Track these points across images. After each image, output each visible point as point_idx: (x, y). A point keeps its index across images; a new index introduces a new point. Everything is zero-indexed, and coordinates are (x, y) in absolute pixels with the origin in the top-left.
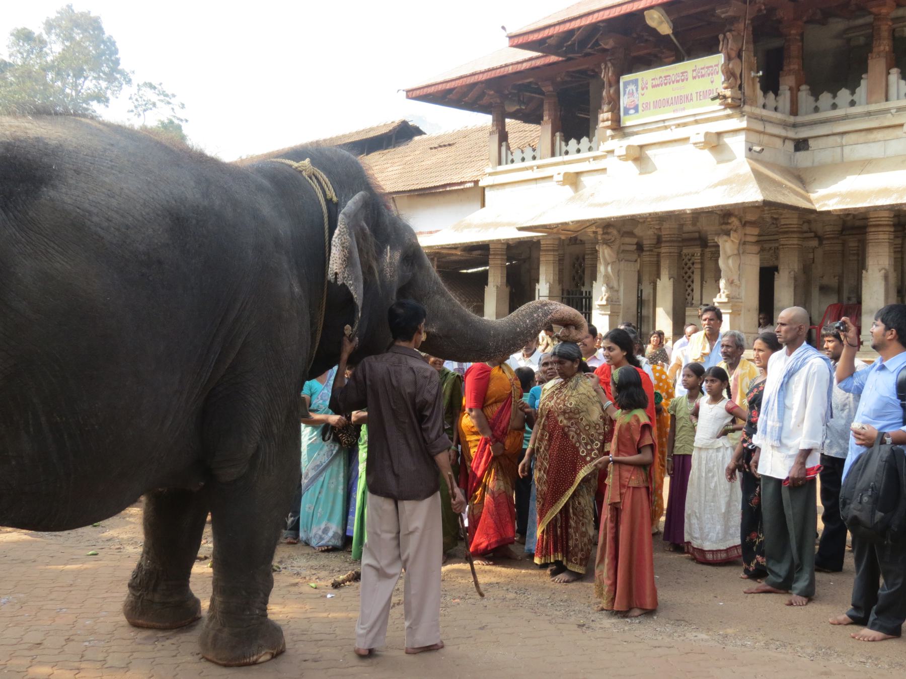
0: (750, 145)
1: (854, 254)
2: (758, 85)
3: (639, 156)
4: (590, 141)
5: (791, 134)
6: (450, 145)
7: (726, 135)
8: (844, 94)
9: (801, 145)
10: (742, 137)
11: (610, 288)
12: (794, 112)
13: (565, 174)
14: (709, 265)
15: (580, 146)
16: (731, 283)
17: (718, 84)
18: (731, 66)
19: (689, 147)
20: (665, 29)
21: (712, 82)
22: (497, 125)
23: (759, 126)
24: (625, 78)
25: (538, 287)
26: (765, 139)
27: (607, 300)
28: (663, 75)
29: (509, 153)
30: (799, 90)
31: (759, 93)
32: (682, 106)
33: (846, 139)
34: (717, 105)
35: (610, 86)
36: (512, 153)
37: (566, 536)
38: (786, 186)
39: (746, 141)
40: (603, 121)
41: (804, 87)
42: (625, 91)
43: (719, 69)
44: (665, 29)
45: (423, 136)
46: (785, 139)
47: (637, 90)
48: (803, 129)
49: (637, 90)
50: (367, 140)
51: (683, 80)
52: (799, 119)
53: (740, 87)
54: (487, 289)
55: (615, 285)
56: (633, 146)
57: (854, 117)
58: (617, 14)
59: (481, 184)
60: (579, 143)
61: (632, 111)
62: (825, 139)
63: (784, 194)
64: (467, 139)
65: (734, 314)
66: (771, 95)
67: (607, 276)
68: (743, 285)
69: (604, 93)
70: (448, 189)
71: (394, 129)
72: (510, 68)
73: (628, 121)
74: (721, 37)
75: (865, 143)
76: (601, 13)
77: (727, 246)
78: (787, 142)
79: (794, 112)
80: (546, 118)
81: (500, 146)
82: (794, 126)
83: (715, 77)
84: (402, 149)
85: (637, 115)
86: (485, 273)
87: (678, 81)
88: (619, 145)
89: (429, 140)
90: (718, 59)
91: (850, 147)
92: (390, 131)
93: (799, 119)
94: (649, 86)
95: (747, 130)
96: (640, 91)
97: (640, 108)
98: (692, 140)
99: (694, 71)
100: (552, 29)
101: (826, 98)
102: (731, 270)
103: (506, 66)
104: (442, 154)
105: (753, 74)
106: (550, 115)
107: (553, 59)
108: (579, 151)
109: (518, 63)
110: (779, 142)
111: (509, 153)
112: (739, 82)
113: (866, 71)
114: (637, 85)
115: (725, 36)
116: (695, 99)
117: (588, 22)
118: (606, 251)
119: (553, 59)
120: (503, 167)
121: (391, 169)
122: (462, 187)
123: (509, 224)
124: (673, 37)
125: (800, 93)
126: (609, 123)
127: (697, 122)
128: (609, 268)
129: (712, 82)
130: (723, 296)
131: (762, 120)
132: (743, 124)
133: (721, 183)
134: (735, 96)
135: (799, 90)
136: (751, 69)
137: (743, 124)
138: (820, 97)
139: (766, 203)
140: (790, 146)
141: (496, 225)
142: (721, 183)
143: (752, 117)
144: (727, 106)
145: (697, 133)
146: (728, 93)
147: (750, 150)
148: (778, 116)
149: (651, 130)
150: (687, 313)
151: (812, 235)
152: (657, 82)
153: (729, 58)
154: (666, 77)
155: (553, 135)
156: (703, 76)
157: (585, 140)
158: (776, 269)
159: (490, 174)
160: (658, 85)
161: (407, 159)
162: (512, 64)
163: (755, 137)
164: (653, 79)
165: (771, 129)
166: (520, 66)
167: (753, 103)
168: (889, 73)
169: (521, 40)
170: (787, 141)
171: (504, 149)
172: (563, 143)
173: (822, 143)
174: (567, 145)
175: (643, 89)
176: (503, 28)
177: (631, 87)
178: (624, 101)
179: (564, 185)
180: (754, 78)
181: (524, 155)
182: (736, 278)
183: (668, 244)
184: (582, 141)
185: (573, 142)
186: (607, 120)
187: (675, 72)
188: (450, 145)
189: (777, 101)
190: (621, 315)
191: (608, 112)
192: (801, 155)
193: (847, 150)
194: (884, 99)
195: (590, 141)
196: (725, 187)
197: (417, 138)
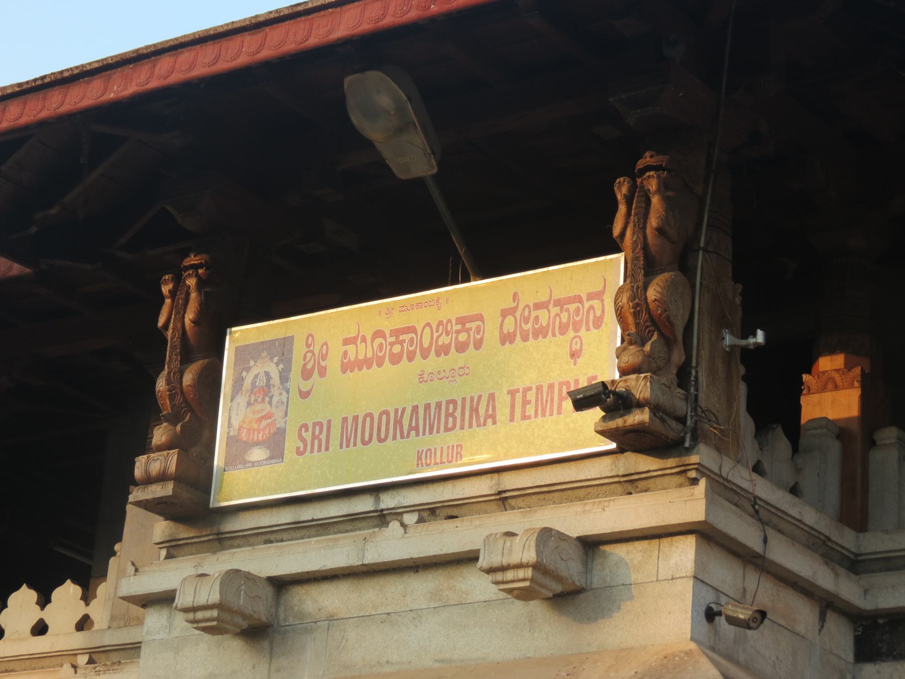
0: (709, 597)
4: (87, 598)
5: (848, 590)
10: (683, 554)
15: (49, 615)
17: (602, 355)
18: (652, 293)
19: (475, 585)
20: (412, 157)
21: (574, 355)
24: (239, 336)
26: (766, 593)
28: (387, 326)
30: (873, 443)
31: (747, 424)
32: (450, 439)
35: (187, 358)
37: (176, 295)
40: (149, 481)
41: (889, 435)
42: (238, 383)
44: (412, 157)
46: (827, 604)
47: (284, 378)
48: (891, 578)
49: (284, 378)
51: (462, 348)
52: (875, 543)
53: (684, 376)
58: (243, 60)
60: (44, 601)
61: (258, 454)
69: (161, 385)
73: (240, 481)
74: (622, 189)
76: (186, 56)
79: (855, 511)
83: (589, 337)
87: (443, 350)
88: (196, 577)
90: (608, 272)
94: (333, 363)
95: (705, 534)
96: (296, 379)
97: (291, 443)
98: (483, 562)
99: (505, 313)
105: (729, 339)
108: (40, 629)
110: (804, 614)
112: (678, 356)
116: (503, 412)
124: (436, 194)
125: (876, 456)
126: (163, 490)
127: (503, 500)
129: (574, 355)
131: (757, 510)
132: (689, 504)
134: (663, 400)
135: (873, 443)
136: (721, 322)
137: (689, 504)
143: (721, 489)
144: (629, 441)
145: (512, 537)
146: (640, 387)
147: (711, 615)
149: (323, 527)
152: (362, 351)
153: (645, 267)
154: (396, 333)
156: (541, 332)
157: (67, 593)
160: (366, 363)
163: (727, 574)
164: (346, 342)
175: (306, 374)
178: (231, 416)
180: (728, 356)
186: (162, 478)
187: (432, 316)
189: (798, 470)
191: (168, 446)
195: (87, 598)
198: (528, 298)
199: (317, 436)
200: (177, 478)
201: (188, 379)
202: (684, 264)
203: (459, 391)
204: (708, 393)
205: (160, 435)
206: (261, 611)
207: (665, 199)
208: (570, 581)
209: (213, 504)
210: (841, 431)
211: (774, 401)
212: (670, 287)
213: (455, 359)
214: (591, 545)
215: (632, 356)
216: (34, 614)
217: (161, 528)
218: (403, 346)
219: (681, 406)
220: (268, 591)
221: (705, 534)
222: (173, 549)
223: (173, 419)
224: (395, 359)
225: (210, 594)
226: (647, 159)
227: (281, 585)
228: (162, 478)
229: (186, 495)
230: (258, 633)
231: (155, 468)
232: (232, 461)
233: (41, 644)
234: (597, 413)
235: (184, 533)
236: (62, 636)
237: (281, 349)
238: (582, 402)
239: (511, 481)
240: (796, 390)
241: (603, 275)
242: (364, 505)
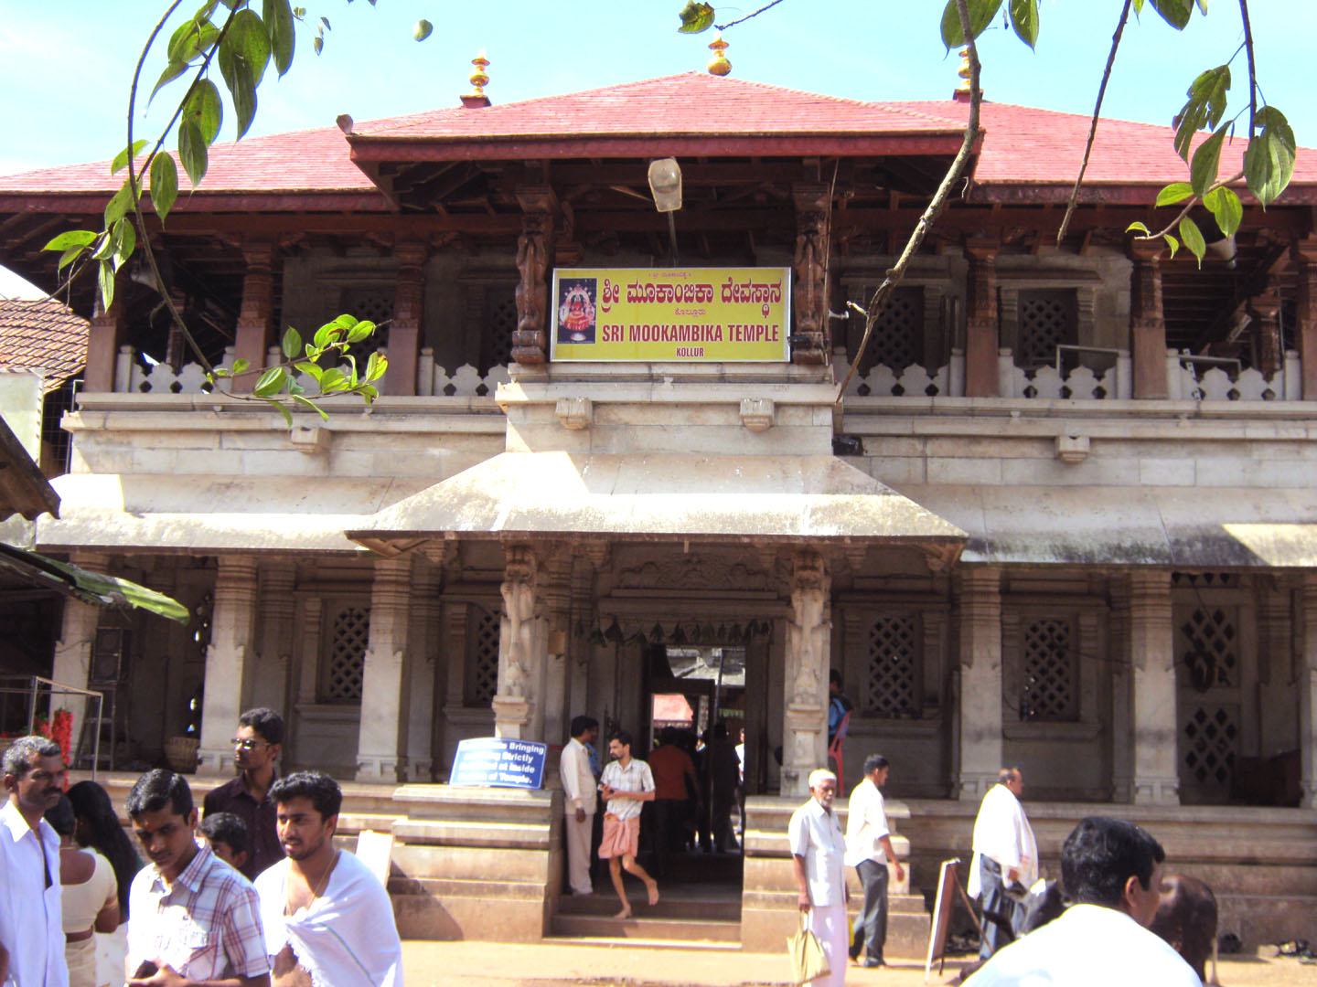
1: (312, 623)
7: (791, 411)
8: (915, 376)
20: (669, 202)
33: (931, 448)
44: (669, 202)
49: (592, 299)
52: (1207, 406)
55: (528, 665)
57: (931, 412)
67: (519, 646)
75: (967, 457)
77: (516, 603)
85: (589, 346)
87: (689, 299)
91: (941, 460)
94: (623, 296)
97: (599, 333)
138: (872, 371)
151: (774, 596)
155: (117, 352)
156: (745, 299)
168: (419, 354)
172: (441, 371)
173: (888, 447)
175: (606, 300)
183: (392, 588)
193: (934, 465)
194: (109, 385)
239: (729, 371)
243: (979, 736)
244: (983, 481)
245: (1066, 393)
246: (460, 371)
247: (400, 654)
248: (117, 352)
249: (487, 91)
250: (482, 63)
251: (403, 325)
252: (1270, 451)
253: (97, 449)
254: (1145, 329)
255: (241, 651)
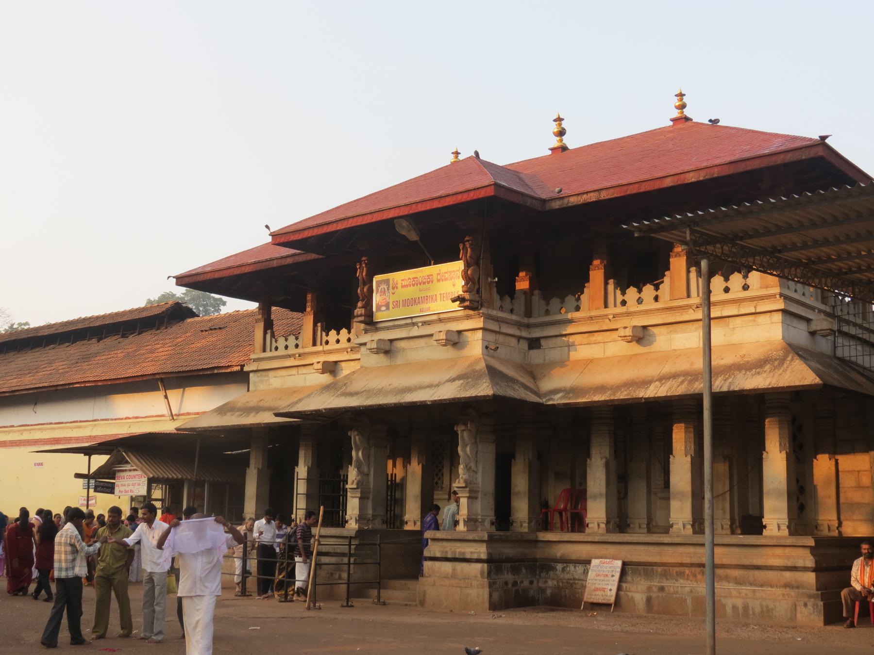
0: (486, 343)
2: (495, 290)
3: (387, 349)
4: (349, 332)
5: (525, 334)
6: (220, 328)
9: (534, 344)
10: (479, 334)
11: (360, 472)
12: (528, 313)
13: (325, 362)
14: (658, 481)
15: (340, 337)
16: (468, 468)
18: (469, 272)
22: (263, 314)
23: (494, 326)
24: (376, 279)
25: (297, 469)
26: (501, 338)
27: (357, 484)
28: (411, 277)
29: (274, 340)
31: (496, 297)
34: (456, 306)
35: (364, 285)
36: (276, 341)
38: (518, 381)
39: (483, 340)
40: (358, 316)
41: (536, 292)
42: (377, 289)
43: (460, 274)
44: (413, 236)
45: (196, 319)
46: (519, 338)
50: (139, 319)
51: (428, 283)
52: (532, 321)
53: (478, 291)
54: (248, 471)
55: (366, 470)
56: (383, 340)
59: (246, 369)
60: (338, 334)
61: (383, 308)
62: (554, 340)
63: (514, 389)
64: (237, 323)
65: (472, 498)
66: (508, 299)
68: (480, 468)
70: (216, 371)
71: (168, 309)
72: (275, 262)
73: (379, 317)
74: (461, 246)
77: (464, 434)
78: (521, 341)
79: (528, 313)
80: (308, 309)
81: (265, 333)
82: (528, 326)
84: (175, 329)
86: (247, 455)
87: (424, 283)
89: (202, 322)
92: (163, 312)
93: (532, 321)
94: (399, 286)
95: (484, 329)
96: (391, 290)
97: (391, 306)
99: (438, 274)
100: (311, 231)
101: (555, 302)
102: (468, 457)
103: (271, 260)
104: (212, 338)
106: (312, 307)
107: (314, 256)
109: (282, 258)
110: (514, 341)
111: (274, 340)
112: (477, 287)
113: (588, 281)
114: (388, 285)
115: (464, 245)
117: (343, 227)
118: (357, 438)
119: (314, 256)
120: (319, 348)
121: (161, 350)
122: (229, 370)
123: (269, 409)
125: (533, 297)
126: (362, 318)
127: (440, 320)
128: (360, 454)
130: (462, 481)
133: (458, 378)
137: (479, 323)
138: (627, 291)
139: (495, 396)
140: (524, 345)
141: (258, 409)
142: (458, 378)
143: (488, 317)
144: (466, 308)
145: (439, 331)
146: (467, 296)
147: (487, 347)
148: (514, 317)
150: (435, 497)
152: (405, 283)
153: (468, 265)
155: (606, 284)
156: (446, 279)
157: (344, 331)
158: (513, 456)
159: (255, 360)
160: (407, 286)
161: (178, 340)
162: (277, 259)
163: (491, 337)
165: (506, 329)
166: (284, 260)
167: (490, 305)
169: (283, 240)
170: (521, 341)
171: (268, 336)
172: (618, 292)
173: (552, 342)
174: (327, 335)
175: (393, 288)
176: (267, 227)
177: (383, 286)
178: (376, 299)
179: (323, 373)
181: (287, 343)
182: (472, 465)
184: (341, 332)
185: (333, 332)
186: (361, 315)
188: (220, 328)
190: (371, 498)
191: (362, 307)
192: (533, 353)
195: (349, 332)
196: (461, 381)
197: (189, 320)
198: (443, 271)
199: (397, 304)
200: (365, 315)
201: (365, 290)
202: (477, 263)
203: (429, 294)
204: (485, 295)
205: (360, 304)
206: (387, 348)
207: (471, 249)
208: (456, 340)
209: (375, 320)
210: (524, 292)
211: (507, 289)
212: (473, 271)
213: (427, 286)
214: (459, 332)
215: (465, 289)
216: (336, 337)
217: (362, 326)
218: (415, 282)
219: (478, 299)
220: (389, 343)
221: (484, 329)
222: (366, 331)
223: (363, 300)
224: (414, 285)
225: (374, 345)
226: (467, 238)
227: (391, 341)
228: (361, 315)
229: (367, 319)
230: (387, 352)
231: (359, 313)
232: (378, 309)
233: (338, 346)
234: (458, 302)
235: (368, 327)
236: (344, 344)
237: (387, 282)
238: (454, 301)
239: (442, 316)
240: (514, 281)
241: (458, 266)
242: (409, 321)
243: (595, 497)
244: (595, 356)
245: (746, 288)
246: (731, 277)
247: (784, 453)
248: (606, 284)
249: (687, 112)
250: (681, 95)
251: (678, 255)
252: (739, 320)
253: (258, 379)
254: (677, 259)
255: (689, 458)
